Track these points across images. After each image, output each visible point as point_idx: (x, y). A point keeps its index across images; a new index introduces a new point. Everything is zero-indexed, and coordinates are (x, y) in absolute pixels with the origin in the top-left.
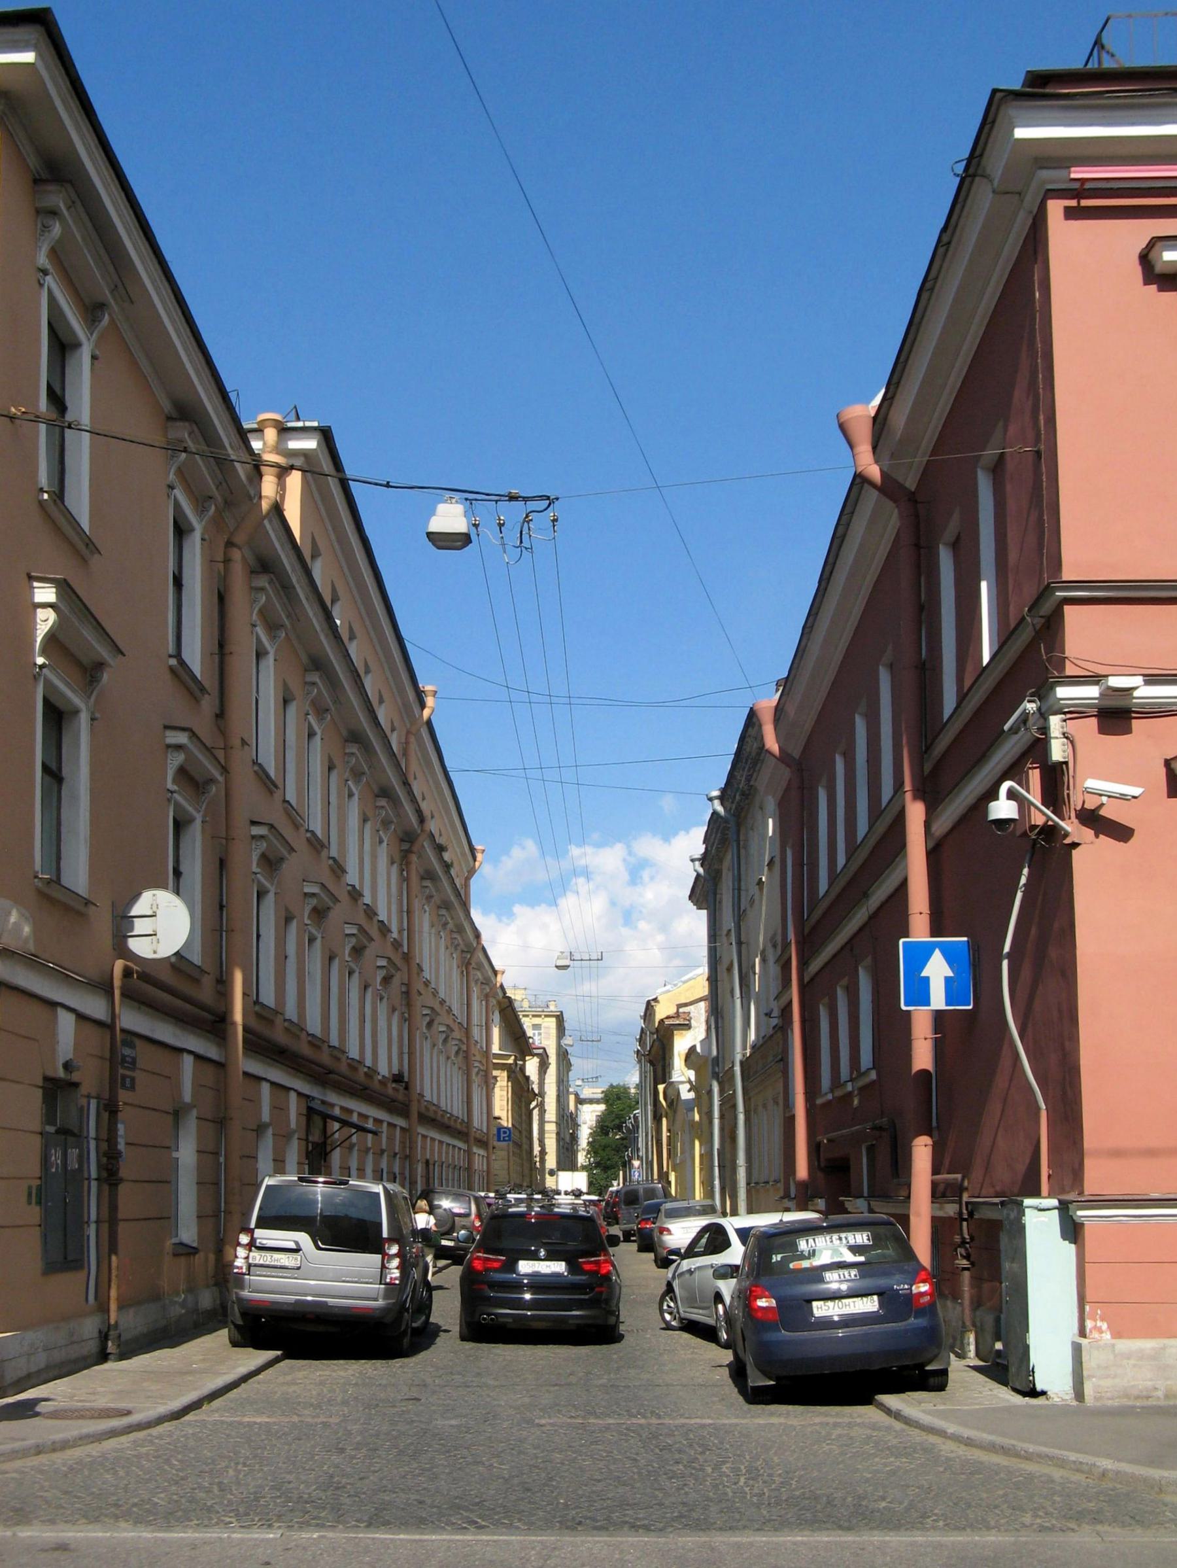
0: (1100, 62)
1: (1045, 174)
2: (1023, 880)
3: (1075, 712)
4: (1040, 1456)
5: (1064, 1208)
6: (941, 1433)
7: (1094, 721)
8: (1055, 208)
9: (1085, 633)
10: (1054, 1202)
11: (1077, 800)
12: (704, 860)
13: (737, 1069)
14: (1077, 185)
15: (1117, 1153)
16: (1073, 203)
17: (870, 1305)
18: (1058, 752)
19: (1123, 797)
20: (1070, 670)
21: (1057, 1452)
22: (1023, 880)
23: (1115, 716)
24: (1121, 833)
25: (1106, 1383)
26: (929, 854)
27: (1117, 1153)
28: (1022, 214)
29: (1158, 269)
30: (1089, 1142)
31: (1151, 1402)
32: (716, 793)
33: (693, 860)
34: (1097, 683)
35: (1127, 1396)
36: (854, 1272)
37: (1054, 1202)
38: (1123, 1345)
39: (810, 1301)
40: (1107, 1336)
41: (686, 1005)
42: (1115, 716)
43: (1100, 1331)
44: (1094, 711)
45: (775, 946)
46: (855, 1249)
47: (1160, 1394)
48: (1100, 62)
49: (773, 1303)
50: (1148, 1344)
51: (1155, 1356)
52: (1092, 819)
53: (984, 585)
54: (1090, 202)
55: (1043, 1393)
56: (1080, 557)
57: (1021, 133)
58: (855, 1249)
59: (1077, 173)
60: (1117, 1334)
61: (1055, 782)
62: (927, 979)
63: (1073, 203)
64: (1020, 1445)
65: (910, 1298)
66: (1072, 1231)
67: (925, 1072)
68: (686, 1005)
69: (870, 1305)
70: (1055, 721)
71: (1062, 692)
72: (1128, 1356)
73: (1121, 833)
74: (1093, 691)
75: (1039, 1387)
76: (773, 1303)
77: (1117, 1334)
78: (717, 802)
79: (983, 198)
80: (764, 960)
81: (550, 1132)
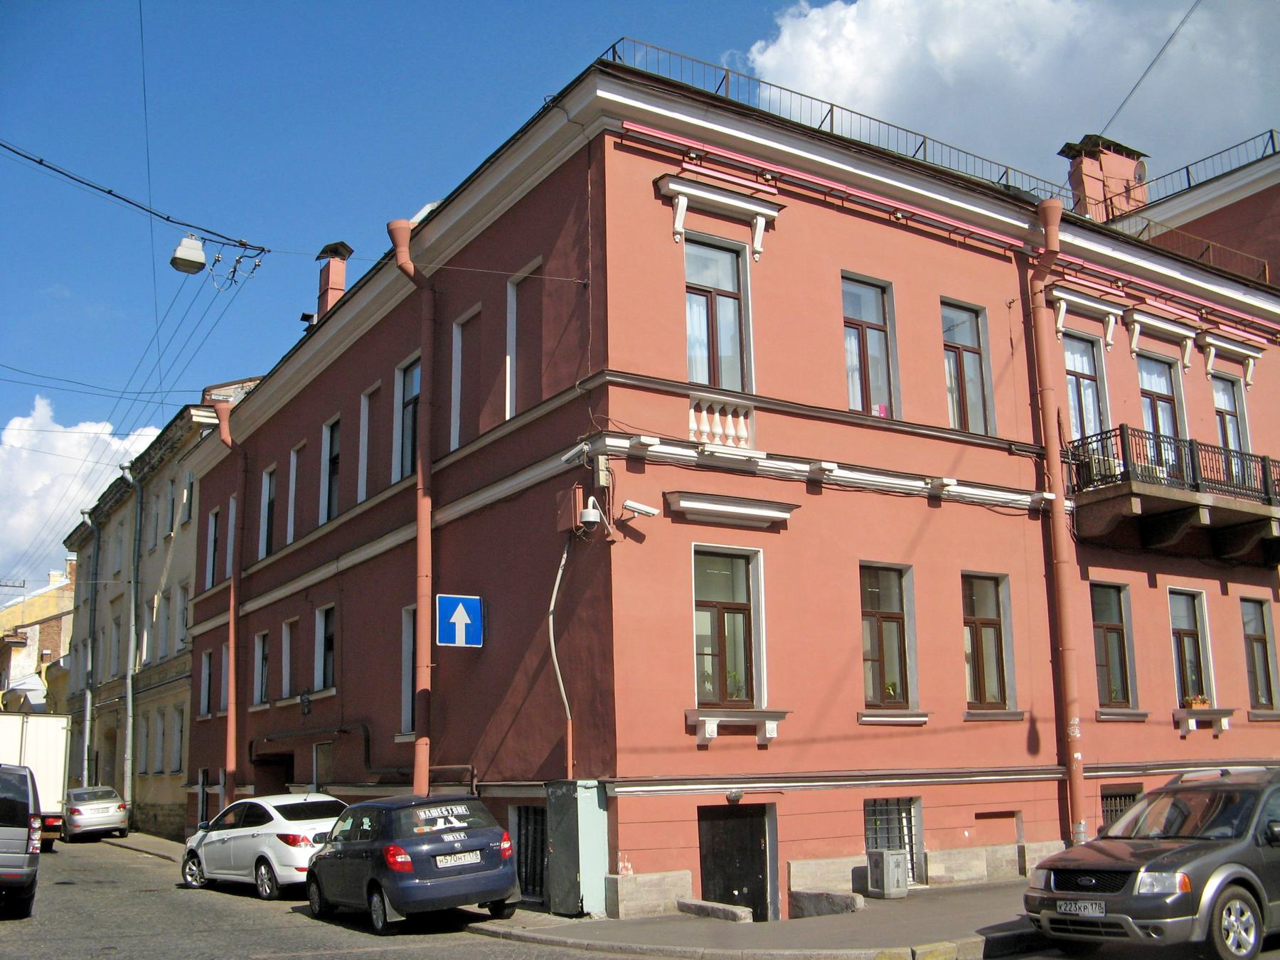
0: (727, 92)
1: (606, 119)
2: (563, 562)
3: (614, 455)
4: (652, 950)
5: (602, 787)
6: (565, 944)
7: (624, 462)
8: (609, 141)
9: (621, 404)
10: (595, 783)
11: (616, 512)
12: (93, 513)
13: (129, 681)
14: (623, 131)
15: (635, 750)
16: (619, 141)
17: (473, 858)
18: (603, 479)
19: (647, 514)
20: (611, 427)
21: (661, 947)
22: (563, 562)
23: (637, 461)
24: (639, 537)
25: (632, 904)
26: (433, 531)
27: (635, 750)
28: (580, 138)
29: (663, 191)
30: (621, 742)
31: (655, 915)
32: (127, 464)
33: (83, 513)
34: (629, 438)
35: (643, 912)
36: (463, 834)
37: (595, 783)
38: (642, 878)
39: (434, 857)
40: (631, 872)
41: (23, 627)
42: (637, 461)
43: (627, 869)
44: (624, 456)
45: (185, 589)
46: (459, 818)
47: (661, 909)
48: (727, 92)
49: (408, 858)
50: (655, 876)
51: (659, 884)
52: (622, 525)
53: (508, 358)
54: (629, 143)
55: (588, 914)
56: (616, 361)
57: (600, 93)
58: (459, 818)
59: (627, 125)
60: (636, 871)
61: (603, 497)
62: (454, 624)
63: (619, 141)
64: (634, 946)
65: (500, 852)
66: (607, 802)
67: (425, 691)
68: (23, 627)
69: (473, 858)
70: (602, 459)
71: (610, 441)
72: (644, 885)
73: (639, 537)
74: (625, 443)
75: (586, 910)
76: (408, 858)
77: (636, 871)
78: (127, 471)
79: (557, 121)
80: (167, 598)
81: (1046, 720)
